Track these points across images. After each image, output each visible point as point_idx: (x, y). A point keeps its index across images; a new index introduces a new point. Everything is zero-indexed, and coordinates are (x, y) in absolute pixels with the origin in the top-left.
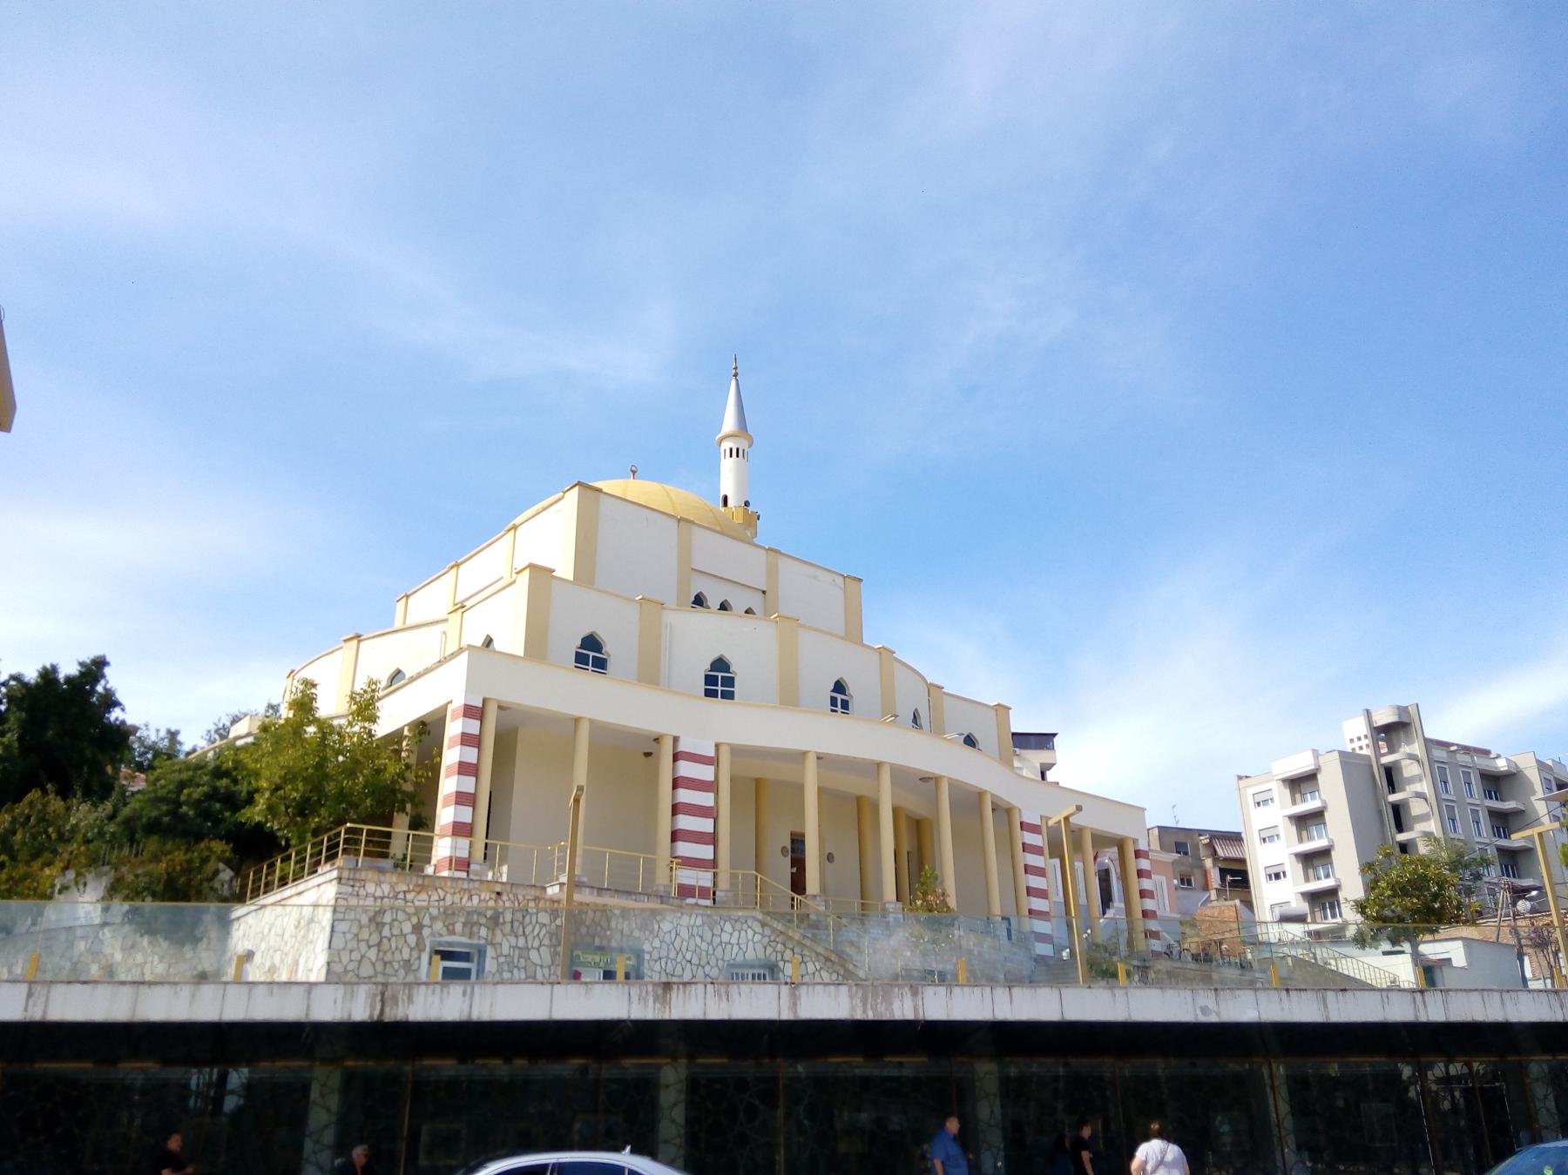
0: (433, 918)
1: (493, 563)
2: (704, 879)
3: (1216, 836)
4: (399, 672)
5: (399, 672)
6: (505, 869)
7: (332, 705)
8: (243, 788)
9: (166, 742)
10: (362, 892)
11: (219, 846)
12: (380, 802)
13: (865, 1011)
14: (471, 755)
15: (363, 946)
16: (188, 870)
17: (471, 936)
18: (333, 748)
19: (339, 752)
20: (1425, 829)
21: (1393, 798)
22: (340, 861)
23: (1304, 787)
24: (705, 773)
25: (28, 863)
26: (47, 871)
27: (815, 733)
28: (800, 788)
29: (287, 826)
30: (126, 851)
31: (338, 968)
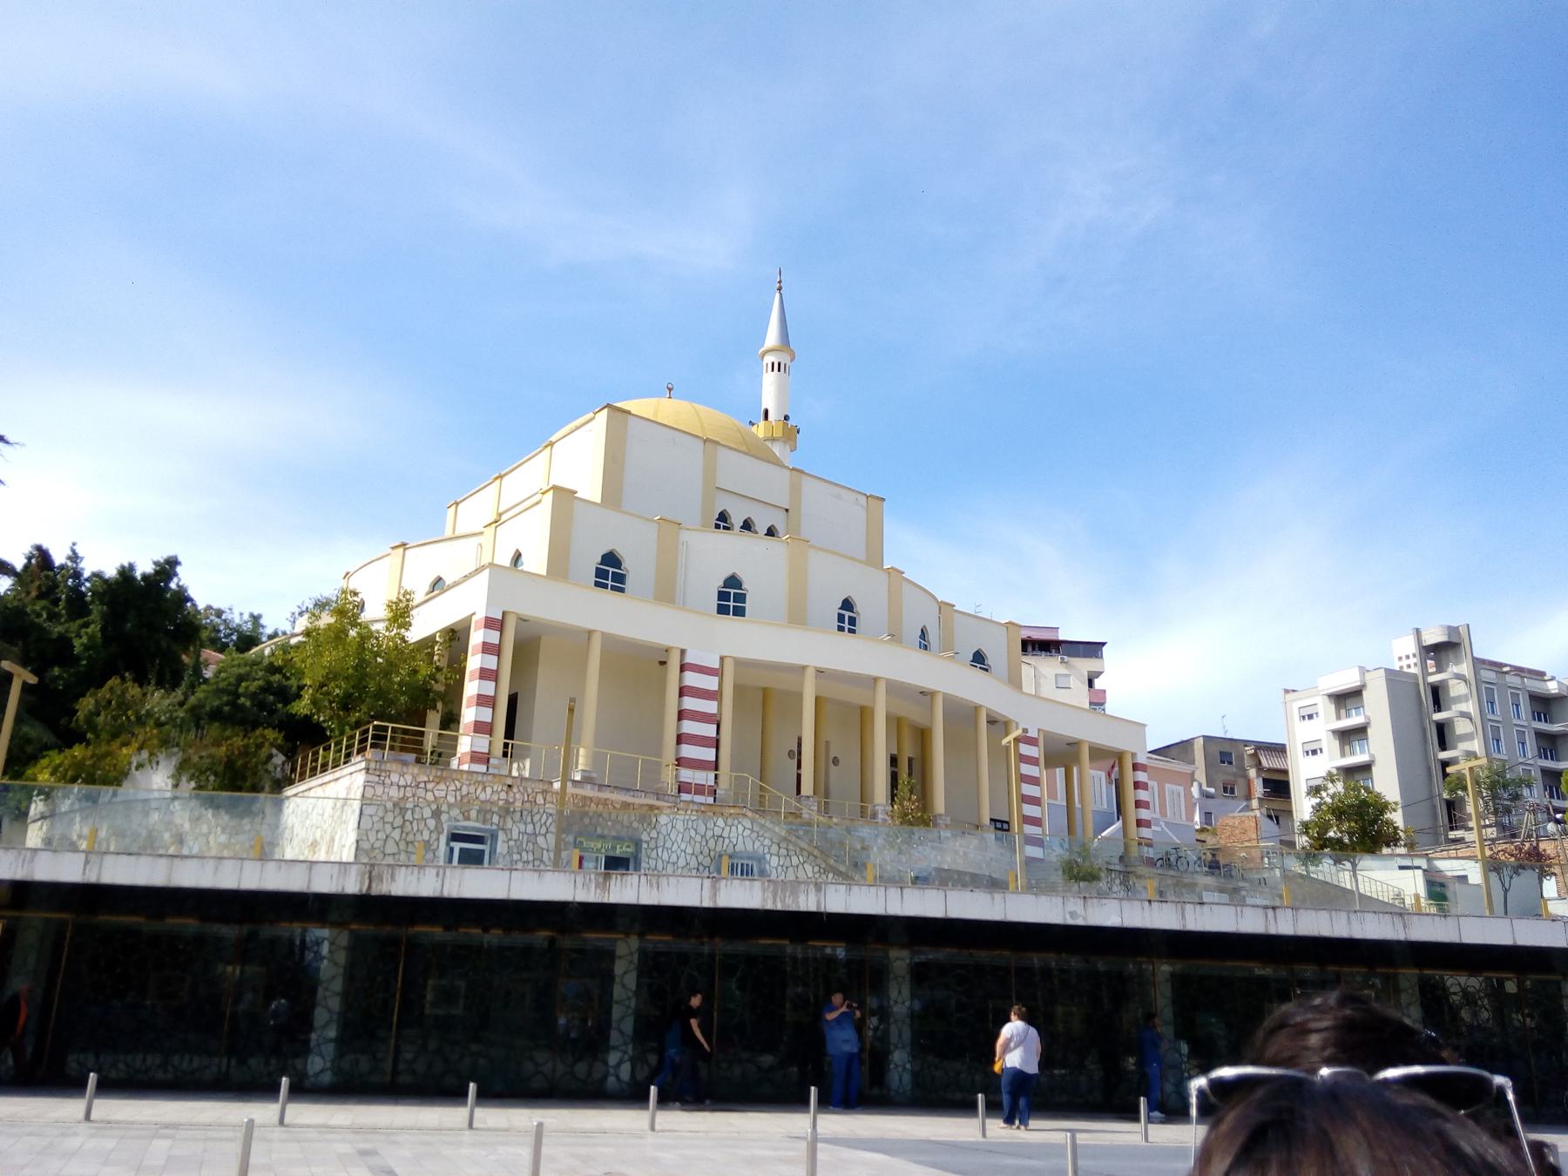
0: (450, 806)
1: (530, 478)
2: (704, 778)
3: (1261, 747)
4: (439, 579)
5: (439, 579)
6: (528, 763)
7: (375, 613)
8: (293, 682)
9: (250, 625)
10: (387, 781)
11: (271, 734)
12: (414, 699)
13: (774, 901)
14: (491, 662)
15: (388, 827)
16: (245, 753)
17: (484, 822)
18: (371, 651)
19: (377, 654)
20: (1470, 750)
21: (1438, 716)
22: (369, 753)
23: (1349, 702)
24: (711, 683)
25: (108, 742)
26: (124, 751)
27: (819, 650)
28: (798, 697)
29: (331, 718)
30: (192, 735)
31: (365, 845)
